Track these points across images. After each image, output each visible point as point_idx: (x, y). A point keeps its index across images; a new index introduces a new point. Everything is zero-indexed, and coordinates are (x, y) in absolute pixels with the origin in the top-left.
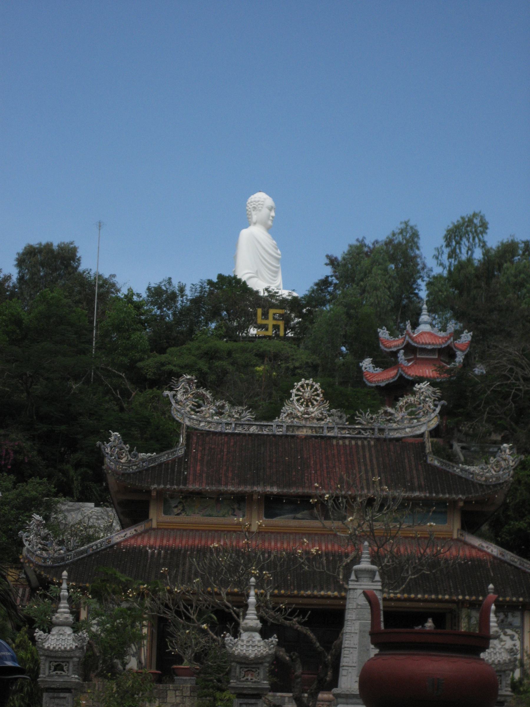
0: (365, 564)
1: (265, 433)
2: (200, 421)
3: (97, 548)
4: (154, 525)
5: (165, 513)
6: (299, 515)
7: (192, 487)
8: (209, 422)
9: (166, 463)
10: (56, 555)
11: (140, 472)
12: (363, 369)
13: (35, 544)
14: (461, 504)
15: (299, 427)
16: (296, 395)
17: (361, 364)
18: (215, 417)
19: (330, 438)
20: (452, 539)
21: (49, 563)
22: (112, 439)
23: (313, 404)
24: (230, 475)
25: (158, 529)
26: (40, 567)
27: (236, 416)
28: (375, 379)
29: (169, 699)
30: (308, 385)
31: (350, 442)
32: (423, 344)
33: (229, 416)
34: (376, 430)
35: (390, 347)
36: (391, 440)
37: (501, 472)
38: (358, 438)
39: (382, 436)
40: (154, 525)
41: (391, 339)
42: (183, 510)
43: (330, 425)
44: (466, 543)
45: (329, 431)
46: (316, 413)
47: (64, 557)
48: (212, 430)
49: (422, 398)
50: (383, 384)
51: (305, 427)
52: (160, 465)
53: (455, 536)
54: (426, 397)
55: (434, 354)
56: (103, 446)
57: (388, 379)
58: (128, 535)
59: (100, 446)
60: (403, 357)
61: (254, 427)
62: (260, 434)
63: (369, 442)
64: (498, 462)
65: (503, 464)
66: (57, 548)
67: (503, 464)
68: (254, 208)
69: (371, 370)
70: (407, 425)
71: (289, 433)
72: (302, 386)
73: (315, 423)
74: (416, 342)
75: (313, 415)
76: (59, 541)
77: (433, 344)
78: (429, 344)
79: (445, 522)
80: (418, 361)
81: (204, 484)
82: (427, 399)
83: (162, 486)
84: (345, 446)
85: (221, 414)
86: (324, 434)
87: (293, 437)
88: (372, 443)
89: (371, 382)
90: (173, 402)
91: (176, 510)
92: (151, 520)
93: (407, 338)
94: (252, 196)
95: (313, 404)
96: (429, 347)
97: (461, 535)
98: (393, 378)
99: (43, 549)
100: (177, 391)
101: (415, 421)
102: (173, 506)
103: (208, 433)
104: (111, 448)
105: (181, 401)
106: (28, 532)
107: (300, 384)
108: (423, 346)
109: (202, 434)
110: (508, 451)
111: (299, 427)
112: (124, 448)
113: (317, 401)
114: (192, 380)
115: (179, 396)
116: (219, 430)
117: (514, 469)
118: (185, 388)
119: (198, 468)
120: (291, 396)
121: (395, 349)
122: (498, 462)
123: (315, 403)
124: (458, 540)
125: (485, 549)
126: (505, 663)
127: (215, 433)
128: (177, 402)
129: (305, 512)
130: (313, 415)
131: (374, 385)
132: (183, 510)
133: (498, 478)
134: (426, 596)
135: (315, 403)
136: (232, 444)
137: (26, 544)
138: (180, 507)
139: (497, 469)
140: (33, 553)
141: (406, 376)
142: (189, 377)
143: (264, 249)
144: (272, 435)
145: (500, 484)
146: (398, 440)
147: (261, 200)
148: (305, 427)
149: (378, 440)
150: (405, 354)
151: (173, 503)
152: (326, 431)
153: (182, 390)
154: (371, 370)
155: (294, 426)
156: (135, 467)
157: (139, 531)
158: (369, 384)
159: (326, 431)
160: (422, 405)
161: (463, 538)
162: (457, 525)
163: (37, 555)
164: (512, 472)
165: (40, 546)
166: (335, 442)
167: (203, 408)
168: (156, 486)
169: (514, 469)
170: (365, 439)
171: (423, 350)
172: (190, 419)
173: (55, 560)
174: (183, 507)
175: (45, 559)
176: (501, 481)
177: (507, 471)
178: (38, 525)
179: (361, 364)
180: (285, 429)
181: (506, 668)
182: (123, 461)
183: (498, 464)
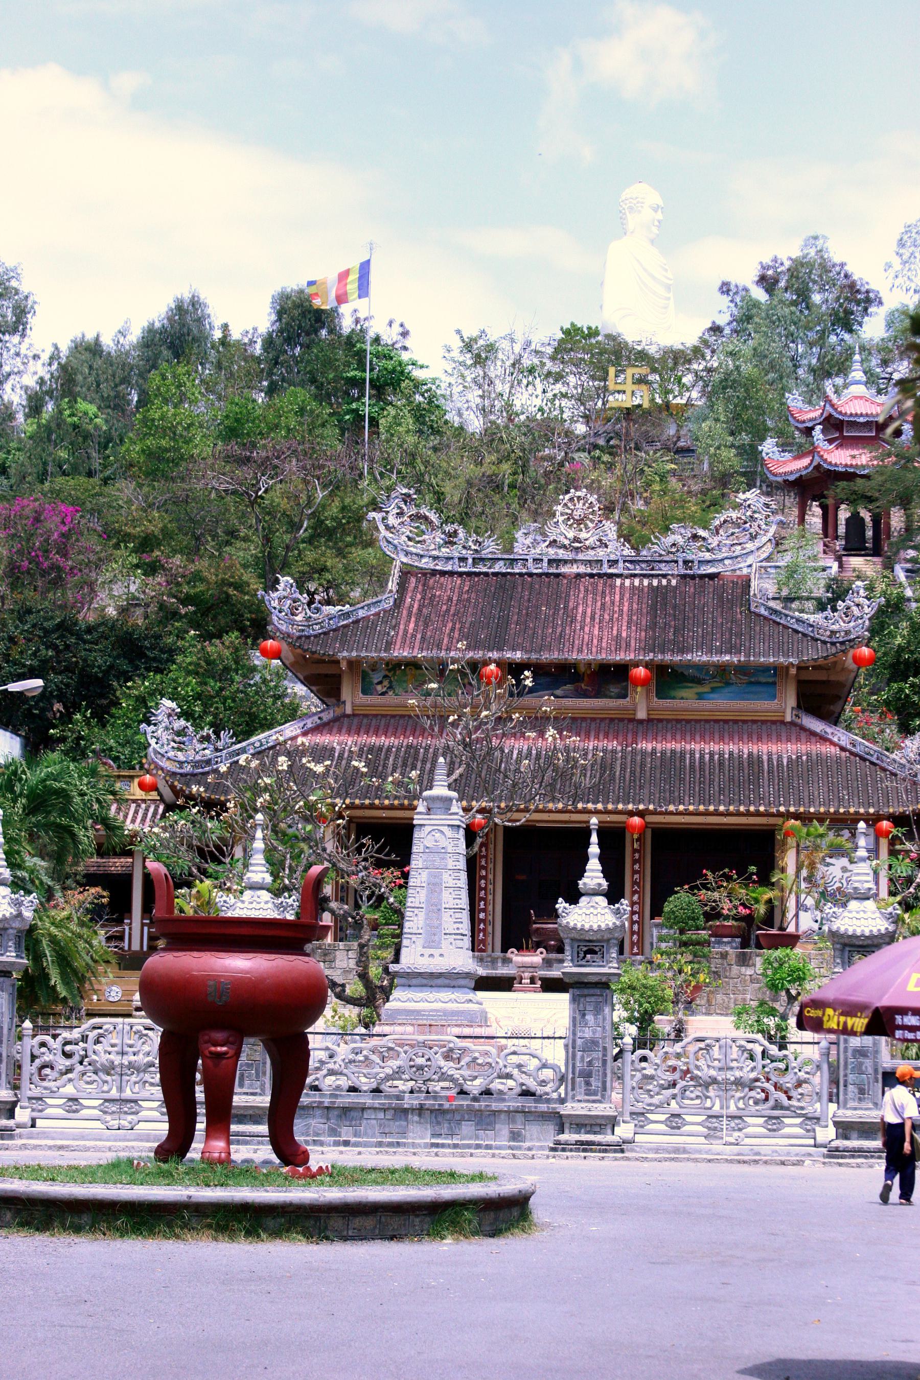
0: (440, 790)
1: (517, 571)
2: (422, 556)
3: (261, 745)
4: (349, 710)
5: (365, 692)
6: (558, 692)
7: (400, 652)
8: (435, 558)
9: (367, 618)
10: (198, 758)
11: (325, 633)
12: (764, 454)
13: (165, 742)
14: (793, 671)
15: (566, 562)
16: (562, 514)
17: (760, 448)
18: (443, 550)
19: (611, 576)
20: (783, 722)
21: (188, 769)
22: (280, 587)
23: (586, 527)
24: (456, 635)
25: (354, 715)
26: (174, 774)
27: (473, 547)
28: (781, 470)
29: (338, 963)
30: (579, 498)
31: (641, 582)
32: (851, 415)
33: (464, 547)
34: (681, 563)
35: (804, 422)
36: (702, 577)
37: (852, 624)
38: (653, 576)
39: (689, 572)
40: (349, 710)
41: (807, 408)
42: (391, 687)
43: (613, 557)
44: (803, 728)
45: (610, 567)
46: (591, 540)
47: (210, 760)
48: (438, 568)
49: (749, 513)
50: (792, 478)
51: (576, 561)
52: (357, 622)
53: (788, 719)
54: (754, 512)
55: (871, 430)
56: (267, 598)
57: (799, 470)
58: (309, 725)
59: (263, 597)
60: (821, 436)
61: (501, 563)
62: (509, 573)
63: (669, 581)
64: (848, 608)
65: (856, 611)
66: (199, 746)
67: (856, 611)
68: (631, 208)
69: (777, 456)
70: (726, 555)
71: (552, 571)
72: (571, 499)
73: (590, 555)
74: (840, 413)
75: (587, 543)
76: (202, 737)
77: (867, 415)
78: (861, 415)
79: (774, 697)
80: (844, 442)
81: (416, 650)
82: (756, 516)
83: (354, 654)
84: (632, 587)
85: (453, 543)
86: (603, 571)
87: (557, 575)
88: (674, 582)
89: (775, 475)
90: (382, 528)
91: (379, 688)
92: (344, 702)
93: (828, 407)
94: (627, 190)
95: (586, 527)
96: (862, 420)
97: (797, 716)
98: (806, 468)
99: (180, 749)
100: (387, 512)
101: (739, 548)
102: (376, 681)
103: (434, 572)
104: (280, 599)
105: (394, 527)
106: (155, 725)
107: (567, 497)
108: (852, 419)
109: (424, 574)
110: (862, 592)
111: (566, 562)
112: (299, 600)
113: (592, 521)
114: (409, 496)
115: (392, 520)
116: (449, 568)
117: (870, 619)
118: (399, 508)
119: (412, 625)
120: (554, 515)
121: (810, 425)
122: (848, 608)
123: (590, 525)
124: (792, 723)
125: (830, 737)
126: (608, 929)
127: (443, 573)
128: (388, 528)
129: (569, 687)
130: (587, 543)
131: (779, 479)
132: (391, 687)
133: (847, 633)
134: (731, 808)
135: (590, 525)
136: (466, 588)
137: (153, 742)
138: (386, 683)
139: (847, 619)
140: (163, 756)
141: (825, 466)
142: (405, 491)
143: (645, 270)
144: (526, 574)
145: (850, 641)
146: (712, 576)
147: (645, 195)
148: (576, 561)
149: (684, 577)
150: (823, 431)
151: (376, 678)
152: (605, 565)
153: (396, 511)
154: (777, 456)
155: (560, 560)
156: (317, 627)
157: (325, 719)
158: (772, 478)
159: (605, 565)
160: (747, 525)
161: (799, 721)
162: (792, 701)
163: (169, 758)
164: (867, 623)
165: (173, 744)
166: (618, 582)
167: (425, 537)
168: (345, 654)
169: (870, 619)
170: (664, 576)
171: (853, 425)
172: (407, 553)
173: (197, 764)
174: (390, 682)
175: (181, 763)
176: (852, 637)
177: (860, 621)
178: (169, 715)
179: (760, 448)
180: (545, 564)
181: (610, 936)
182: (299, 618)
183: (847, 612)
